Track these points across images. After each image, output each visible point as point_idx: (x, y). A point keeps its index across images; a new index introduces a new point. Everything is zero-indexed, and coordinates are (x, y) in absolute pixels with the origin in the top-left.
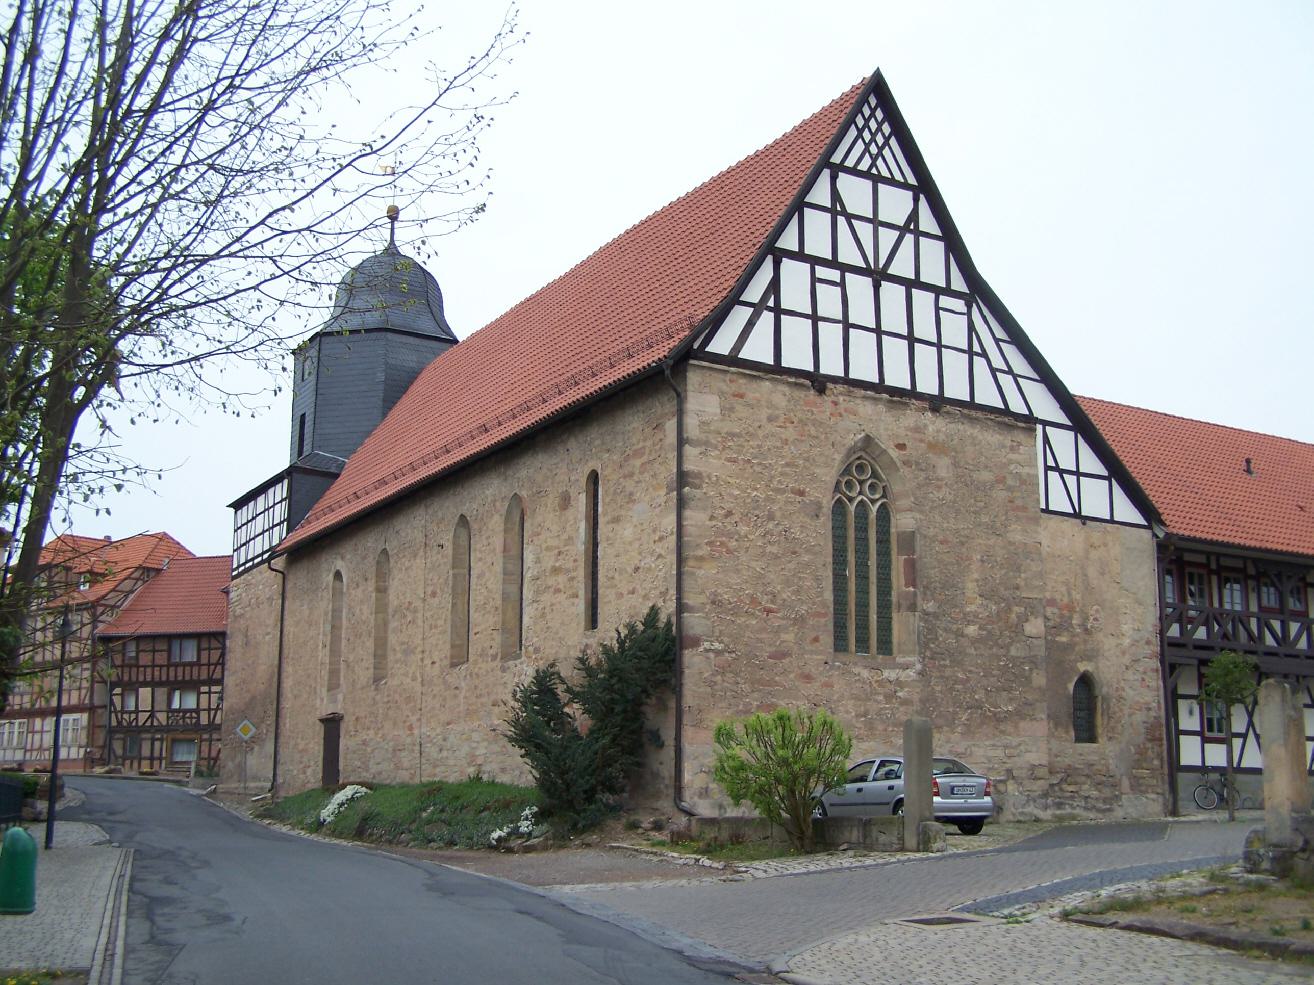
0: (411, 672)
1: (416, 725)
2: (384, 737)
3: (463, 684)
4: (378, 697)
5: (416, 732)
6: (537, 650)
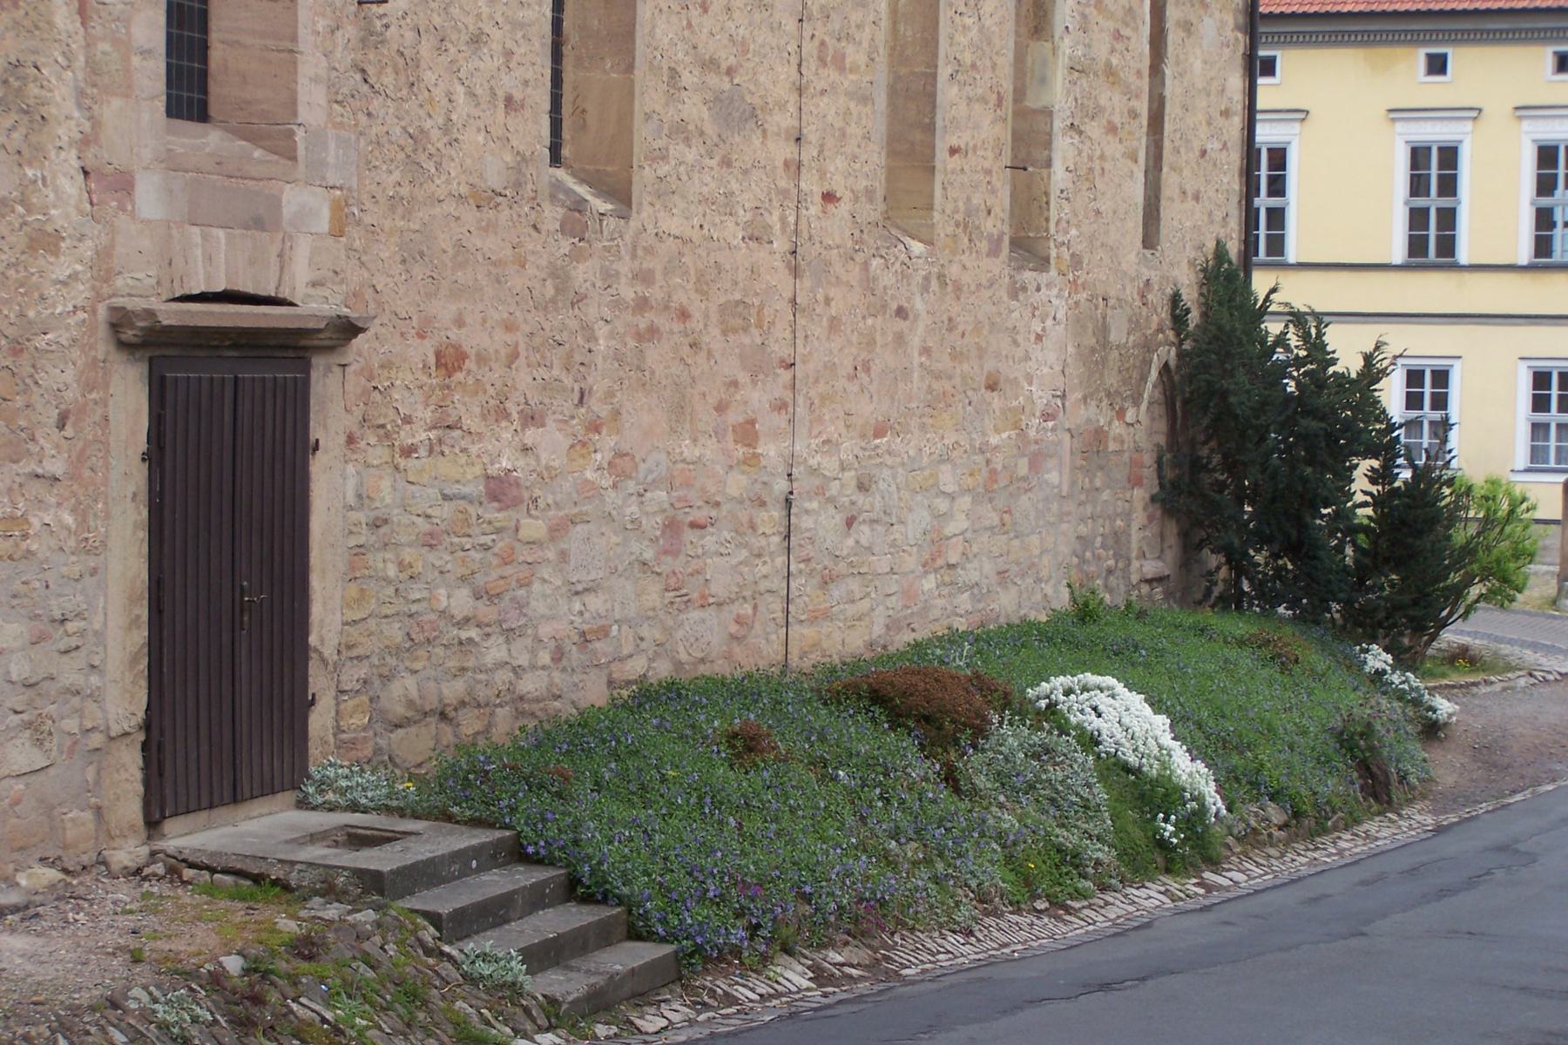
0: (747, 199)
1: (769, 422)
2: (620, 468)
3: (919, 304)
4: (583, 274)
5: (770, 450)
6: (1076, 261)
